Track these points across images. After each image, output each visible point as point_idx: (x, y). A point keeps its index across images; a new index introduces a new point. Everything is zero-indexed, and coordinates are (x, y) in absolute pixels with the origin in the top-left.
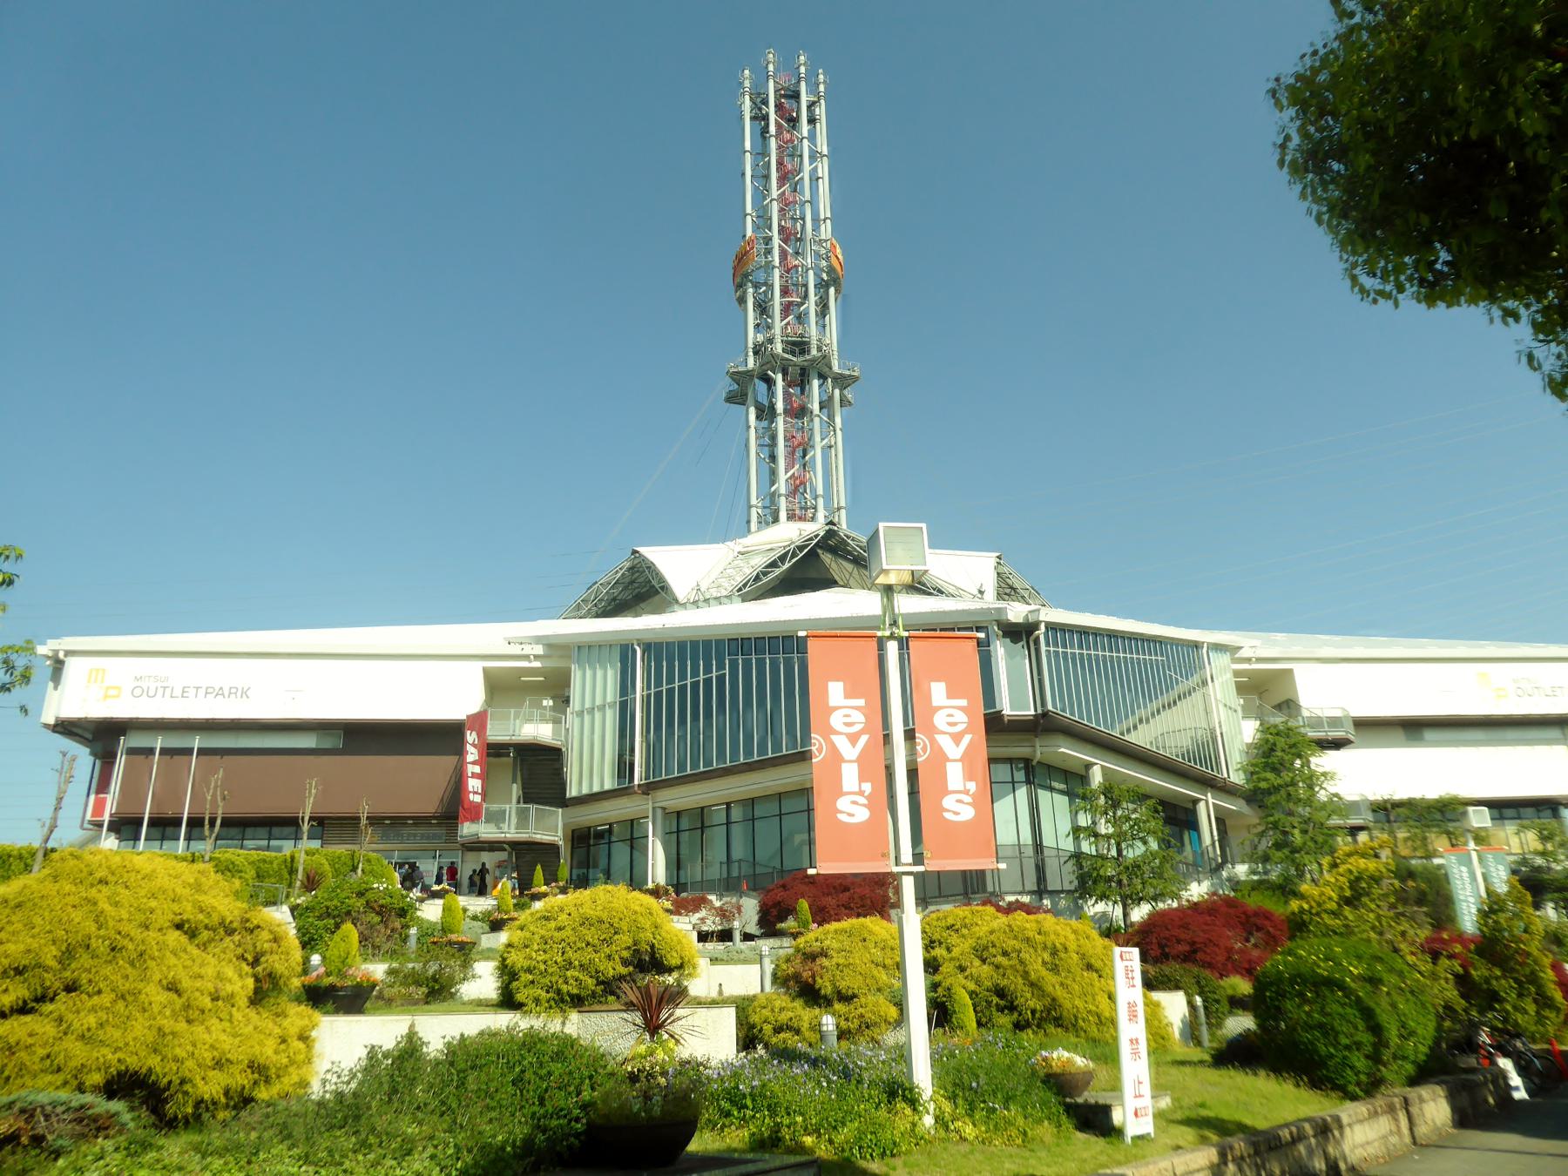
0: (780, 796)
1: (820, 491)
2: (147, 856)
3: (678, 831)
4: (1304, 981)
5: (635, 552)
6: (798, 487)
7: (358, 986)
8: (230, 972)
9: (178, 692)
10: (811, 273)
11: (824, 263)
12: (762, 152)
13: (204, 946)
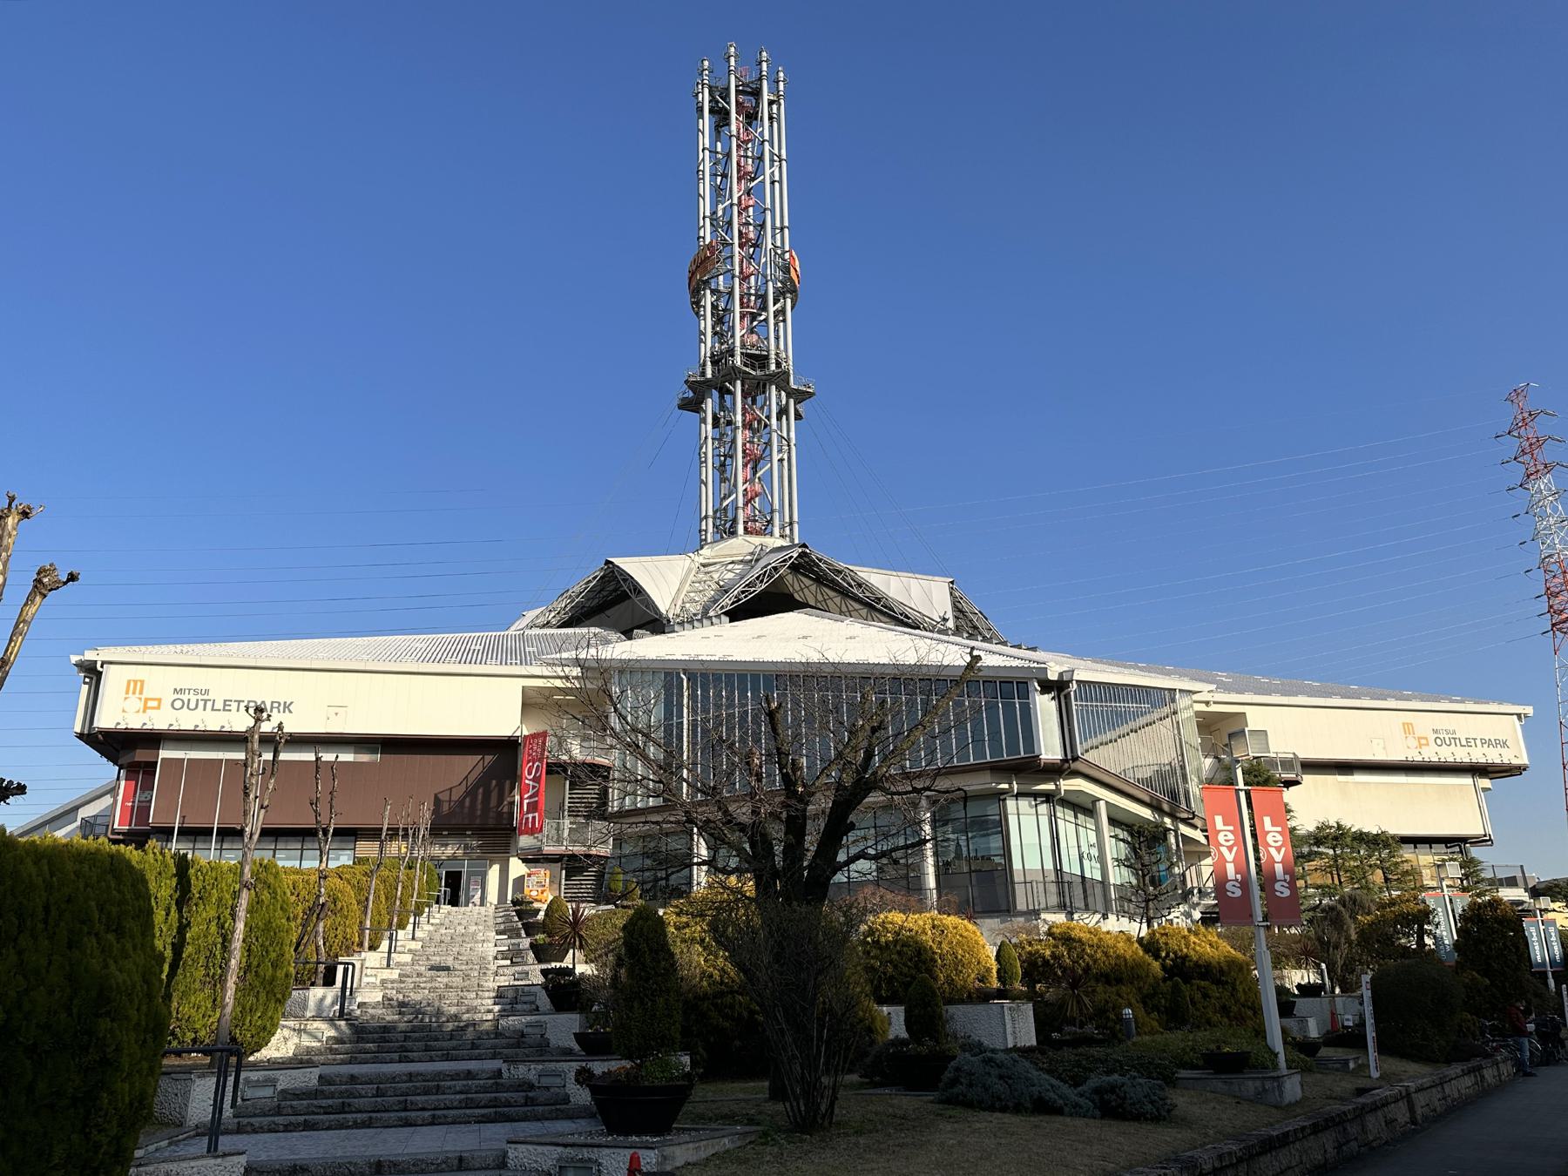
5: (608, 562)
9: (219, 705)
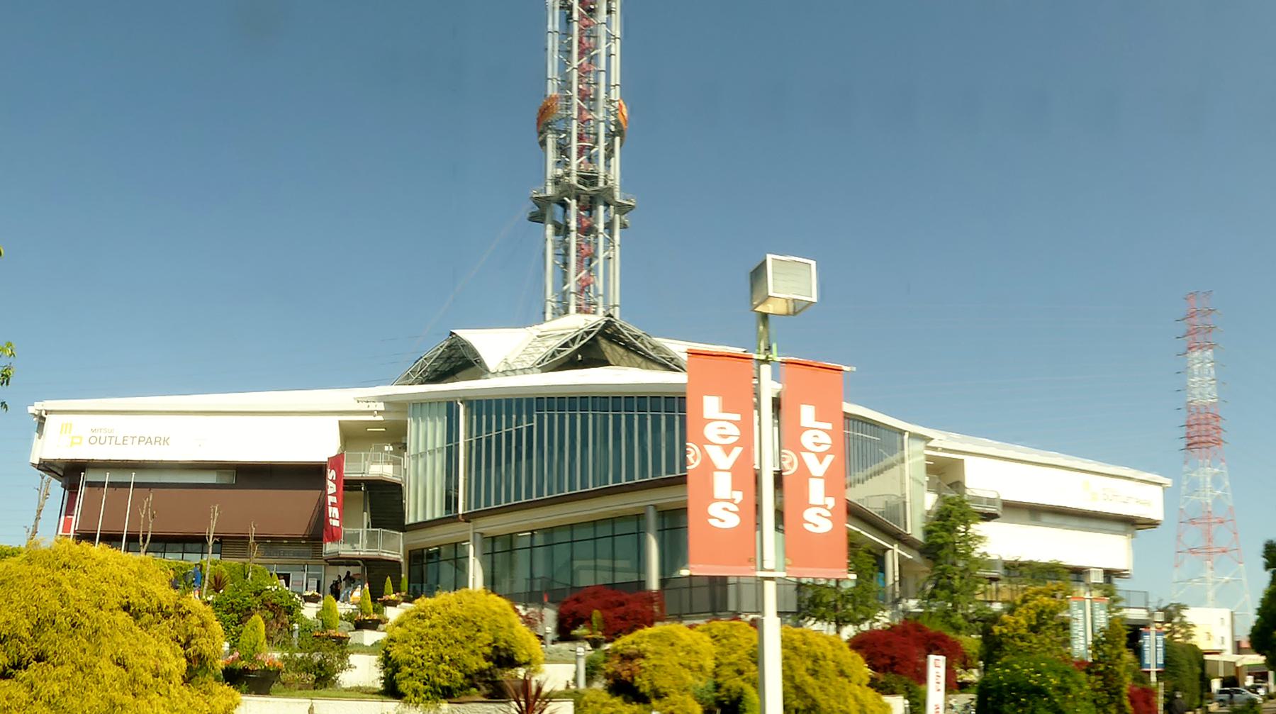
0: (572, 526)
1: (601, 292)
2: (98, 550)
3: (493, 553)
4: (1019, 690)
5: (452, 333)
6: (584, 288)
7: (266, 671)
8: (167, 652)
10: (602, 125)
11: (612, 118)
12: (566, 33)
13: (146, 627)
